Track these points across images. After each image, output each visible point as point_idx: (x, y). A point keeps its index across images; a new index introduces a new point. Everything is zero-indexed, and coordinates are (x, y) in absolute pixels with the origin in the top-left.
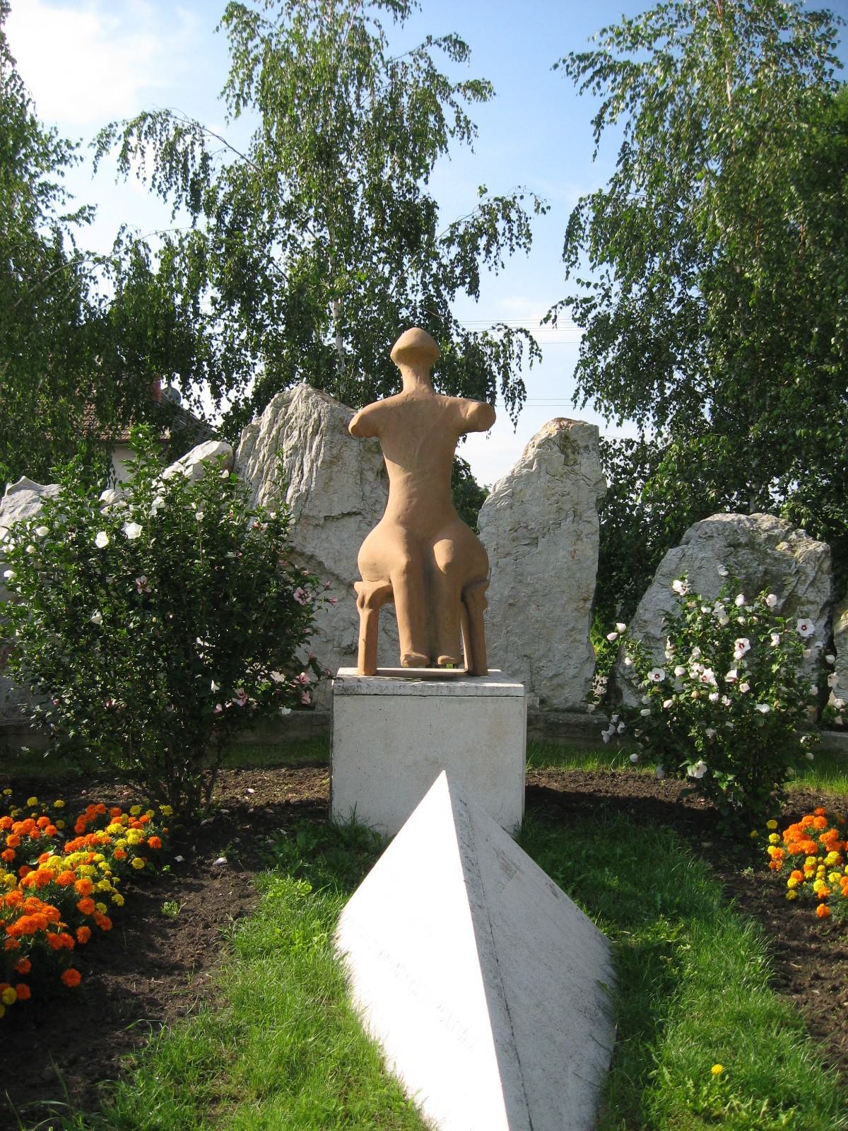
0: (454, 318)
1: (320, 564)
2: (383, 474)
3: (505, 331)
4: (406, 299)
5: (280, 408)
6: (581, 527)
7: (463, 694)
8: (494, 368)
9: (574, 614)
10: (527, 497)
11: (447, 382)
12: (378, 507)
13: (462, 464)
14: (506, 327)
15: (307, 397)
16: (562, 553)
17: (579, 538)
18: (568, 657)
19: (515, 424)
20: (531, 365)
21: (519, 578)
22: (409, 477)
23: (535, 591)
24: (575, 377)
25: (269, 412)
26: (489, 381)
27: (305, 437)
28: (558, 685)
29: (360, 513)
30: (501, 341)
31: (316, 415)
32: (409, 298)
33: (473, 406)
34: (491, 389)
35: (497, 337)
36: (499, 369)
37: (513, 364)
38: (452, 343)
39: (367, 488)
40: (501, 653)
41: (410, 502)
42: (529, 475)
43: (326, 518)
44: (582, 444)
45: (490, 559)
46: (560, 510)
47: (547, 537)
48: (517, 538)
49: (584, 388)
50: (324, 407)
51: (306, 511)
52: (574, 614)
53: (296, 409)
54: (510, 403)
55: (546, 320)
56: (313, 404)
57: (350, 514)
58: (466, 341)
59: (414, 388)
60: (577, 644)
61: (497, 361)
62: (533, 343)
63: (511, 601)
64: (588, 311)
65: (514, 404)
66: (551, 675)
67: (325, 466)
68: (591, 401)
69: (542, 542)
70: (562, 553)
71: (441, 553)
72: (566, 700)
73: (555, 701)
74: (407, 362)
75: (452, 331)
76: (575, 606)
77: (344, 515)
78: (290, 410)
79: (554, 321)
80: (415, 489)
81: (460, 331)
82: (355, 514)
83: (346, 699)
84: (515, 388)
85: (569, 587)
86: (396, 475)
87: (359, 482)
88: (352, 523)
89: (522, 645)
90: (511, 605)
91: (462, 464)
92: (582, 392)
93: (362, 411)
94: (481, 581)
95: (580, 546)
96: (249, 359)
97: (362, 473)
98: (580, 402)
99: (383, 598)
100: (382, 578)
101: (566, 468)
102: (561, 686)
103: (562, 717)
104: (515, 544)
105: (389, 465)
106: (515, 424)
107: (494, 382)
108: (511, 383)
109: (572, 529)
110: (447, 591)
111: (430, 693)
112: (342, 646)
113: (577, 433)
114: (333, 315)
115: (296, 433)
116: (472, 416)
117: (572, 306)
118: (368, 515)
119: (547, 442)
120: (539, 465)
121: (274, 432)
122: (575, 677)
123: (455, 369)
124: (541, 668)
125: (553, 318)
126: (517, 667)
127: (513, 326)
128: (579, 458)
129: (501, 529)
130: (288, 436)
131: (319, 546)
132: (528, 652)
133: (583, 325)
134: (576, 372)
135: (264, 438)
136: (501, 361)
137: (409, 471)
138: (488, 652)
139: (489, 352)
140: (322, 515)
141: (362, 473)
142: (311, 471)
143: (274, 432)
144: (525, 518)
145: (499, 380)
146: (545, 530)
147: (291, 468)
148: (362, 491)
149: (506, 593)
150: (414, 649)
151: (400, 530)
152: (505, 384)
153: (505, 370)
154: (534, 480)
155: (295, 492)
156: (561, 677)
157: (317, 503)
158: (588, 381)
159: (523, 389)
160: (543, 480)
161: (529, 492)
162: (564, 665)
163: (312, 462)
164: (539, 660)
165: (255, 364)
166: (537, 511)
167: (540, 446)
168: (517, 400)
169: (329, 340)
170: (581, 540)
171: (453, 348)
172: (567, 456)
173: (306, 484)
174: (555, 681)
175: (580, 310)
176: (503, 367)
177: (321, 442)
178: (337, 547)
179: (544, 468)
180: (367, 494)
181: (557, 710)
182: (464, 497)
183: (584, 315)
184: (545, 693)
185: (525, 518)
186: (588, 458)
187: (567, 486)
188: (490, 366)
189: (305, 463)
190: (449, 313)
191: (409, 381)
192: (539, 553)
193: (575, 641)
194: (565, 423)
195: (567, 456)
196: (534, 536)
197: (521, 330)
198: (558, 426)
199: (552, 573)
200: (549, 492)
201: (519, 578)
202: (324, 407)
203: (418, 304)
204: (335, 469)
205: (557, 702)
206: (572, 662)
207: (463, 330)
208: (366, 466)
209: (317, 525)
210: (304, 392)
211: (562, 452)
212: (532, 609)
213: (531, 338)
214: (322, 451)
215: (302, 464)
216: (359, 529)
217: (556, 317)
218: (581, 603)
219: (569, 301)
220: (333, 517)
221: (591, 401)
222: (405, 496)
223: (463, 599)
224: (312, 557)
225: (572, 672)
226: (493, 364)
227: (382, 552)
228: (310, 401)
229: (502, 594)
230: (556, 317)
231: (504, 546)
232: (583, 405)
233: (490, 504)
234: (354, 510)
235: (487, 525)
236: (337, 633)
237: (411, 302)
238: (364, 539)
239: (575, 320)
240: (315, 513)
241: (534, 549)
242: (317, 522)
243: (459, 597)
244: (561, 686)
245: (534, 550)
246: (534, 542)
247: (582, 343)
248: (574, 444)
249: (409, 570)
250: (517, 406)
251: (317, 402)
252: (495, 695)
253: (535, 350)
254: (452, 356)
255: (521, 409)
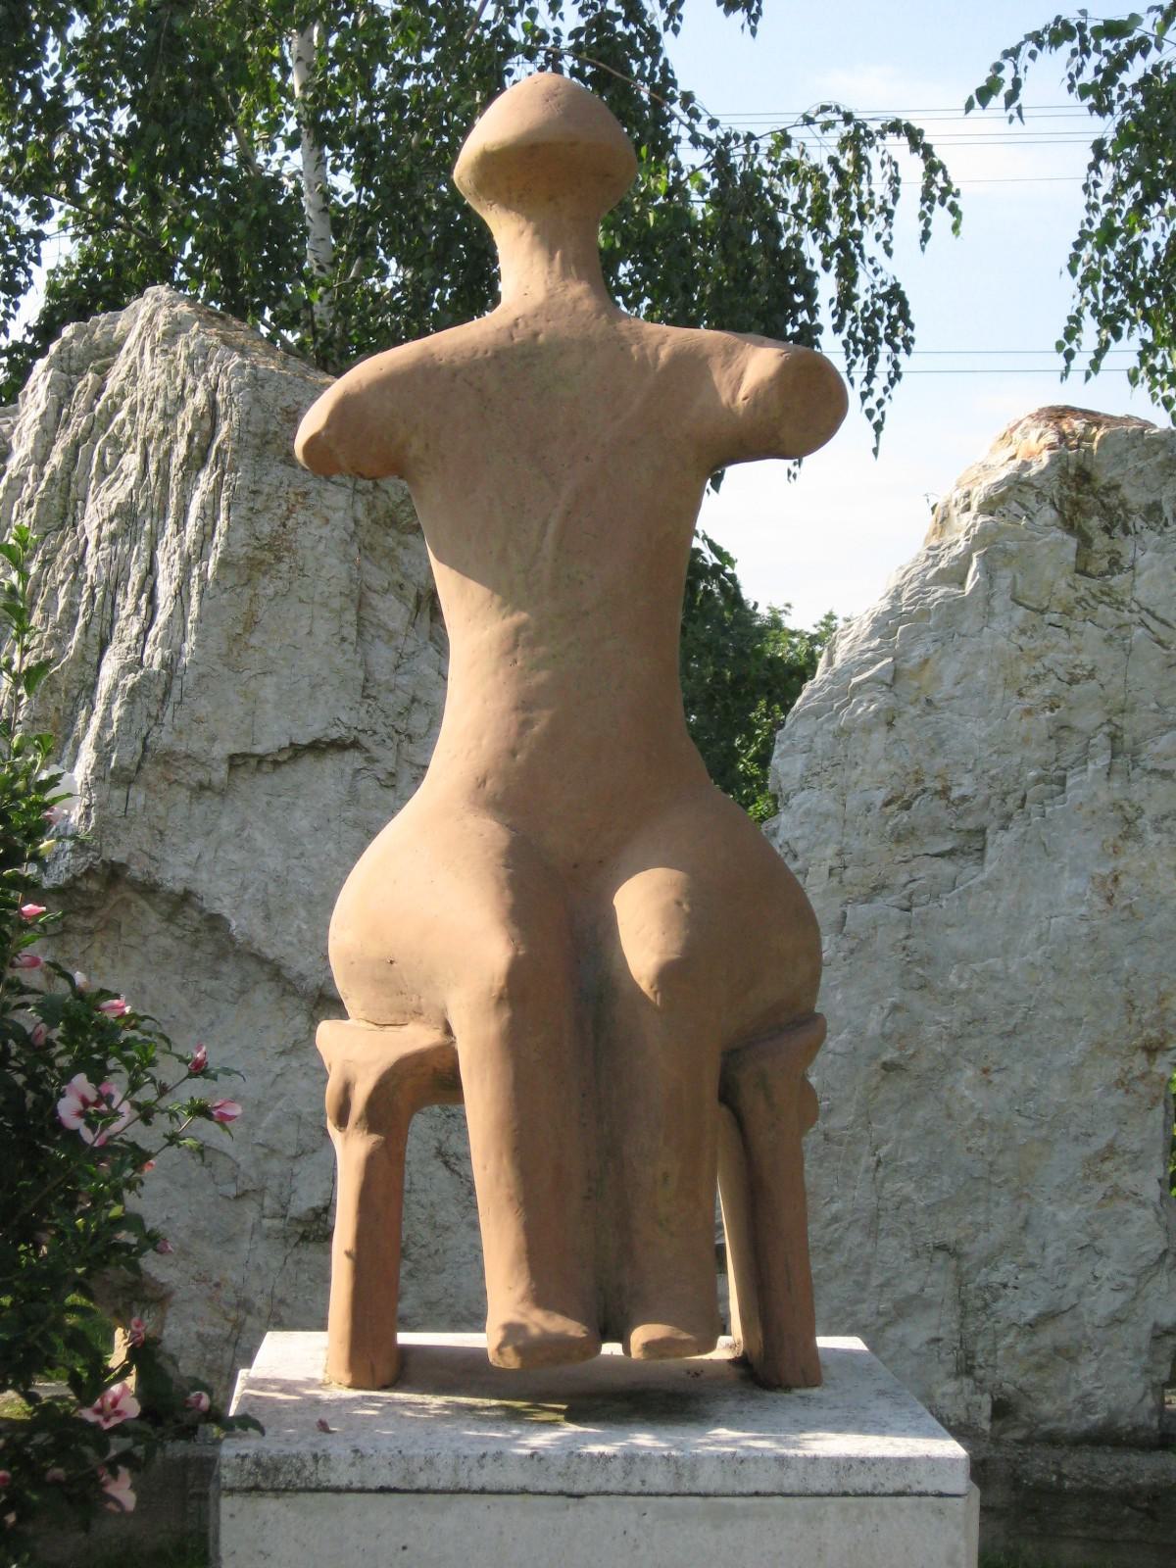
0: (683, 86)
1: (215, 922)
2: (428, 604)
3: (843, 129)
4: (530, 29)
5: (80, 373)
6: (1138, 792)
7: (732, 1485)
8: (811, 250)
9: (1112, 1101)
10: (947, 687)
11: (660, 291)
12: (418, 721)
13: (711, 559)
14: (848, 118)
15: (171, 336)
16: (1070, 885)
17: (1129, 829)
18: (1090, 1249)
19: (878, 427)
20: (926, 236)
21: (919, 972)
22: (519, 630)
23: (979, 1019)
24: (1073, 273)
25: (42, 388)
26: (796, 289)
27: (163, 474)
28: (1057, 1350)
29: (355, 745)
30: (833, 161)
31: (199, 399)
32: (540, 23)
33: (760, 362)
34: (803, 316)
35: (819, 149)
36: (827, 251)
37: (869, 234)
38: (678, 168)
39: (382, 656)
40: (855, 1237)
41: (526, 724)
42: (954, 609)
43: (235, 761)
44: (1135, 496)
45: (816, 904)
46: (1061, 730)
47: (1017, 828)
48: (912, 831)
49: (1095, 312)
50: (228, 370)
51: (163, 739)
52: (1112, 1101)
53: (133, 375)
54: (862, 361)
55: (984, 94)
56: (190, 359)
57: (318, 748)
58: (721, 164)
59: (538, 294)
60: (1121, 1206)
61: (820, 225)
62: (933, 168)
63: (890, 1055)
64: (1119, 64)
65: (873, 361)
66: (1032, 1313)
67: (231, 578)
68: (1125, 352)
69: (1000, 843)
70: (1070, 885)
71: (643, 922)
72: (1086, 1404)
73: (1047, 1408)
74: (513, 200)
75: (675, 129)
76: (1114, 1069)
77: (297, 751)
78: (112, 384)
79: (1012, 97)
80: (543, 676)
81: (702, 129)
82: (339, 746)
83: (269, 1505)
84: (878, 314)
85: (1095, 1003)
86: (473, 625)
87: (351, 633)
88: (328, 777)
89: (930, 1210)
90: (888, 1067)
91: (711, 559)
92: (1090, 324)
93: (337, 388)
94: (798, 1022)
95: (1132, 859)
96: (26, 223)
97: (361, 604)
98: (1081, 361)
99: (424, 1084)
100: (417, 1013)
101: (1083, 583)
102: (1066, 1354)
103: (1076, 1466)
104: (903, 851)
105: (446, 581)
106: (878, 427)
107: (811, 294)
108: (862, 288)
109: (1104, 798)
110: (666, 1069)
111: (598, 1482)
112: (293, 1212)
113: (1120, 459)
114: (294, 81)
115: (131, 461)
116: (758, 398)
117: (1067, 47)
118: (378, 755)
119: (1011, 495)
120: (989, 572)
121: (57, 458)
122: (1116, 1321)
123: (685, 252)
124: (996, 1291)
125: (1008, 86)
126: (911, 1286)
127: (872, 109)
128: (1127, 547)
129: (853, 801)
130: (103, 472)
131: (213, 859)
132: (951, 1235)
133: (1102, 108)
134: (1075, 259)
135: (23, 478)
136: (834, 226)
137: (518, 606)
138: (814, 1230)
139: (792, 196)
140: (221, 750)
141: (361, 604)
142: (181, 595)
143: (57, 458)
144: (940, 762)
145: (827, 286)
146: (1012, 803)
147: (115, 585)
148: (364, 664)
149: (873, 1027)
150: (541, 1297)
151: (486, 833)
152: (846, 300)
153: (846, 257)
154: (969, 623)
155: (126, 669)
156: (1067, 1321)
157: (203, 707)
158: (1110, 290)
159: (904, 314)
160: (999, 625)
161: (951, 669)
162: (1075, 1281)
163: (187, 564)
164: (989, 1261)
165: (39, 236)
166: (981, 737)
167: (989, 506)
168: (885, 349)
169: (285, 162)
170: (1139, 837)
171: (677, 188)
172: (1086, 541)
173: (166, 642)
174: (1046, 1337)
175: (1095, 59)
176: (841, 243)
177: (216, 491)
178: (274, 863)
179: (1004, 582)
180: (383, 674)
181: (1052, 1439)
182: (729, 671)
183: (1109, 76)
184: (1010, 1375)
185: (940, 762)
186: (1160, 549)
187: (1088, 645)
188: (797, 240)
189: (162, 566)
190: (665, 69)
191: (524, 272)
192: (987, 885)
193: (1115, 1193)
194: (1078, 425)
195: (1086, 541)
196: (970, 823)
197: (895, 127)
198: (1051, 437)
199: (1036, 956)
200: (1024, 668)
201: (919, 972)
202: (228, 370)
203: (566, 43)
204: (268, 587)
205: (1052, 1408)
206: (1106, 1269)
207: (713, 124)
208: (378, 578)
209: (203, 787)
210: (161, 319)
211: (1070, 526)
212: (965, 1084)
213: (927, 152)
214: (222, 524)
215: (151, 570)
216: (354, 797)
217: (1017, 83)
218: (1139, 1061)
219: (1061, 32)
220: (261, 759)
221: (1125, 352)
222: (505, 702)
223: (727, 1094)
224: (187, 897)
225: (1105, 1302)
226: (807, 236)
227: (417, 912)
228: (180, 349)
229: (858, 1032)
230: (1017, 83)
231: (863, 861)
232: (1095, 366)
233: (816, 713)
234: (334, 733)
235: (805, 784)
236: (275, 1166)
237: (543, 36)
238: (371, 834)
239: (1084, 91)
240: (196, 745)
241: (971, 869)
242: (201, 775)
243: (710, 1090)
244: (1066, 1354)
245: (974, 875)
246: (973, 845)
247: (1094, 167)
248: (1112, 500)
249: (519, 992)
250: (883, 367)
251: (205, 351)
252: (857, 1487)
253: (938, 191)
254: (678, 215)
255: (896, 377)
